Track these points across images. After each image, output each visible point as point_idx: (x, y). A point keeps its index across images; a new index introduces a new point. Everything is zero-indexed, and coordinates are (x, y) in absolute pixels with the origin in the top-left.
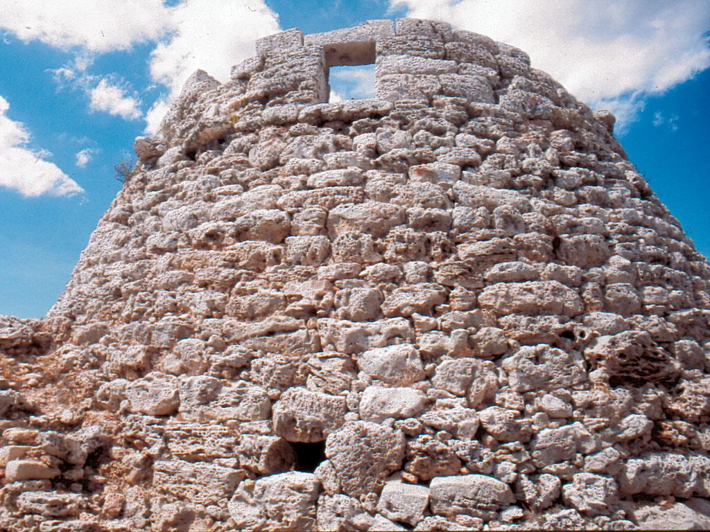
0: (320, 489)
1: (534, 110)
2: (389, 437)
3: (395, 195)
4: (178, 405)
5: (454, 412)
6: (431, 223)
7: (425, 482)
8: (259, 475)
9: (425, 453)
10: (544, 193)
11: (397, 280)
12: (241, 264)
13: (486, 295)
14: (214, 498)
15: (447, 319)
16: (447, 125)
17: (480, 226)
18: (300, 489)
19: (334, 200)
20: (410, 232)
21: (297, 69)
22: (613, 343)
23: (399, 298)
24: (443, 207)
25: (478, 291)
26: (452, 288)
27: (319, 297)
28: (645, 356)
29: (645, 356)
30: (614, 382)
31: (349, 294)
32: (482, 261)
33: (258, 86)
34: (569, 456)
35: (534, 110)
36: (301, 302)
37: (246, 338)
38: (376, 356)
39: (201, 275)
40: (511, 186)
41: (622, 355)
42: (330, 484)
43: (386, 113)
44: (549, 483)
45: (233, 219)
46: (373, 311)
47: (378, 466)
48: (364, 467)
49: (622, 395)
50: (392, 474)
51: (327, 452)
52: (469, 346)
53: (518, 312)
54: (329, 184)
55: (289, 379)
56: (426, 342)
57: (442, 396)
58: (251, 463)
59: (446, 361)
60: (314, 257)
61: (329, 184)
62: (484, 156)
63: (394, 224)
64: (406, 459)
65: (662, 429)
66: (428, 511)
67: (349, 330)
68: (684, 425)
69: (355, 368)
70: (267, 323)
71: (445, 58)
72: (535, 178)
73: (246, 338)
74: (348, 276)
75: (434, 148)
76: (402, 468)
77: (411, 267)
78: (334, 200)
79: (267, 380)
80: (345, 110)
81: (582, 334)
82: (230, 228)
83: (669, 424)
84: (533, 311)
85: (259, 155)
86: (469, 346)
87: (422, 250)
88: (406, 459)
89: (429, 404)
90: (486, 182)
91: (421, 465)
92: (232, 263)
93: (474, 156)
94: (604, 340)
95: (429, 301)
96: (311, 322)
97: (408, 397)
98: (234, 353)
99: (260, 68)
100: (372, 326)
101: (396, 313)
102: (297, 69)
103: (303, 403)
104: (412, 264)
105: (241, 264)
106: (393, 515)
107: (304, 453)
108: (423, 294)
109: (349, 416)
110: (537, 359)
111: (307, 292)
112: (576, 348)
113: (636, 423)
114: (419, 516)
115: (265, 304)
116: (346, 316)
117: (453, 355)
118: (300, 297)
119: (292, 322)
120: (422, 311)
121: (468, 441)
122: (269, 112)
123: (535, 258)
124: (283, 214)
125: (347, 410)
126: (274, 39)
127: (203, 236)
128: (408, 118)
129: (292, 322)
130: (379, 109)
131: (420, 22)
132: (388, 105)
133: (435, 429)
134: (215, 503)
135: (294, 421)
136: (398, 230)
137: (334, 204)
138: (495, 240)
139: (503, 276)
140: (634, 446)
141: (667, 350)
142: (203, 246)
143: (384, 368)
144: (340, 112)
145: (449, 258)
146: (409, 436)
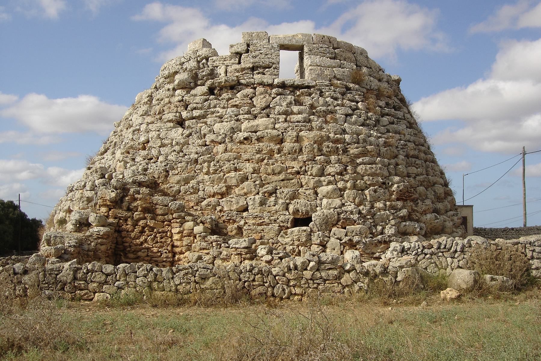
0: (311, 231)
1: (370, 87)
2: (333, 214)
3: (324, 128)
4: (248, 207)
5: (350, 207)
6: (336, 141)
7: (345, 228)
8: (288, 228)
9: (344, 219)
10: (376, 128)
11: (329, 162)
12: (264, 152)
13: (360, 169)
14: (272, 237)
15: (347, 177)
16: (339, 96)
17: (355, 143)
18: (305, 231)
19: (301, 129)
20: (331, 144)
21: (269, 56)
22: (398, 187)
23: (330, 169)
24: (341, 134)
25: (356, 168)
26: (347, 166)
27: (301, 168)
28: (408, 192)
29: (408, 192)
30: (398, 199)
31: (312, 167)
32: (358, 156)
33: (247, 61)
34: (385, 221)
35: (370, 87)
36: (294, 169)
37: (273, 182)
38: (323, 190)
39: (245, 156)
40: (363, 125)
41: (400, 191)
42: (315, 229)
43: (313, 87)
44: (379, 228)
45: (256, 132)
46: (322, 173)
47: (328, 224)
48: (326, 223)
49: (400, 204)
50: (334, 226)
51: (313, 219)
52: (354, 187)
53: (368, 175)
54: (297, 122)
55: (294, 196)
56: (340, 185)
57: (346, 202)
58: (285, 224)
59: (347, 191)
60: (295, 151)
61: (297, 122)
62: (354, 110)
63: (325, 141)
64: (338, 220)
65: (411, 215)
66: (346, 235)
67: (315, 180)
68: (418, 214)
69: (316, 193)
70: (282, 176)
71: (334, 58)
72: (372, 122)
73: (273, 182)
74: (310, 160)
75: (335, 107)
76: (337, 224)
77: (333, 158)
78: (301, 129)
79: (285, 197)
80: (296, 83)
81: (388, 183)
82: (254, 136)
83: (414, 214)
84: (373, 175)
85: (259, 102)
86: (354, 187)
87: (336, 151)
88: (338, 220)
89: (343, 205)
90: (355, 123)
91: (343, 222)
92: (259, 152)
93: (350, 112)
94: (396, 186)
95: (340, 170)
96: (298, 176)
97: (337, 202)
98: (270, 188)
99: (247, 51)
100: (322, 178)
101: (329, 174)
102: (269, 56)
103: (300, 204)
104: (333, 157)
105: (264, 152)
106: (336, 237)
107: (303, 220)
108: (338, 168)
109: (318, 209)
110: (375, 191)
111: (296, 165)
112: (386, 188)
113: (404, 212)
114: (343, 237)
115: (279, 169)
116: (311, 175)
117: (349, 189)
118: (294, 167)
119: (291, 176)
120: (338, 174)
121: (357, 215)
122: (257, 78)
123: (373, 156)
124: (280, 133)
125: (317, 207)
126: (254, 35)
127: (242, 138)
128: (323, 90)
129: (291, 176)
130: (311, 85)
131: (324, 36)
132: (314, 83)
133: (346, 212)
134: (273, 239)
135: (298, 211)
136: (326, 143)
137: (301, 131)
138: (360, 149)
139: (363, 162)
140: (403, 219)
141: (414, 190)
142: (241, 142)
143: (328, 193)
144: (293, 84)
145: (507, 238)
146: (339, 214)
